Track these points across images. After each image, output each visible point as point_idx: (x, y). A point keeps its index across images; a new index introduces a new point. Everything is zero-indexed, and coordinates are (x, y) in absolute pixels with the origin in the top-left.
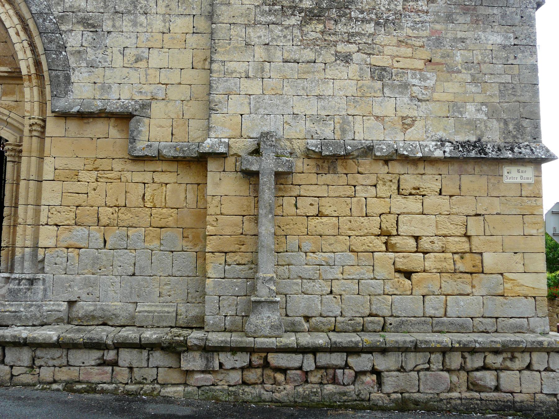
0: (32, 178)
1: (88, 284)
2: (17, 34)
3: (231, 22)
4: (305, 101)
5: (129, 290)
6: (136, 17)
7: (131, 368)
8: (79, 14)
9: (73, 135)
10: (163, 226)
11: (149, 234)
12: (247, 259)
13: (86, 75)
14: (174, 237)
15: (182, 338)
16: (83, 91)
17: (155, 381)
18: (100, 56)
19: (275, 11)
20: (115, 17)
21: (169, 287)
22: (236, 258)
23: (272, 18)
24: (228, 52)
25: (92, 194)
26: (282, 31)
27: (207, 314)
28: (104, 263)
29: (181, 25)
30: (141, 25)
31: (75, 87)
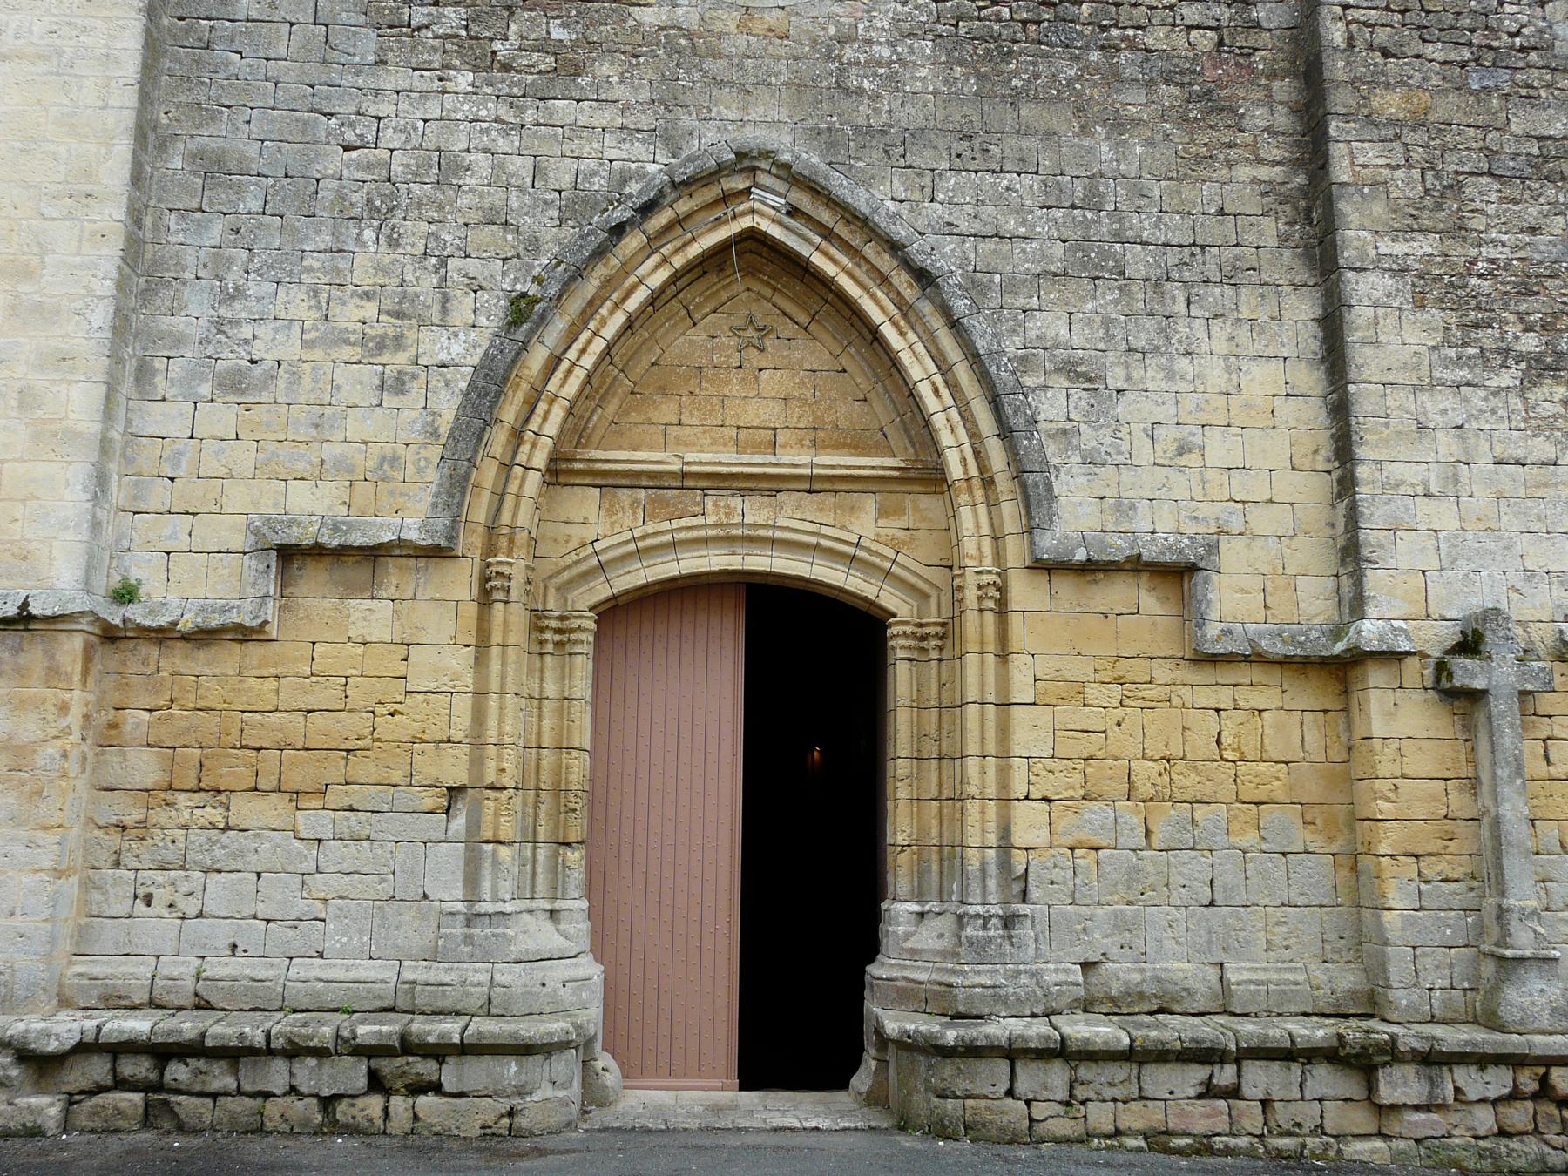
0: (991, 699)
1: (1122, 924)
2: (936, 391)
3: (1385, 380)
4: (1545, 544)
5: (1205, 937)
6: (1171, 360)
7: (1266, 1103)
8: (1057, 352)
9: (1068, 607)
10: (1264, 799)
11: (1236, 817)
12: (1462, 870)
13: (1082, 480)
14: (1285, 822)
15: (1386, 1037)
16: (1079, 516)
17: (1320, 1130)
18: (1108, 440)
19: (1469, 358)
20: (1130, 360)
21: (1284, 929)
22: (1439, 868)
23: (1464, 374)
24: (1385, 442)
25: (1114, 732)
26: (1486, 399)
27: (1395, 985)
28: (1151, 879)
29: (1261, 378)
30: (1182, 377)
31: (1062, 506)
